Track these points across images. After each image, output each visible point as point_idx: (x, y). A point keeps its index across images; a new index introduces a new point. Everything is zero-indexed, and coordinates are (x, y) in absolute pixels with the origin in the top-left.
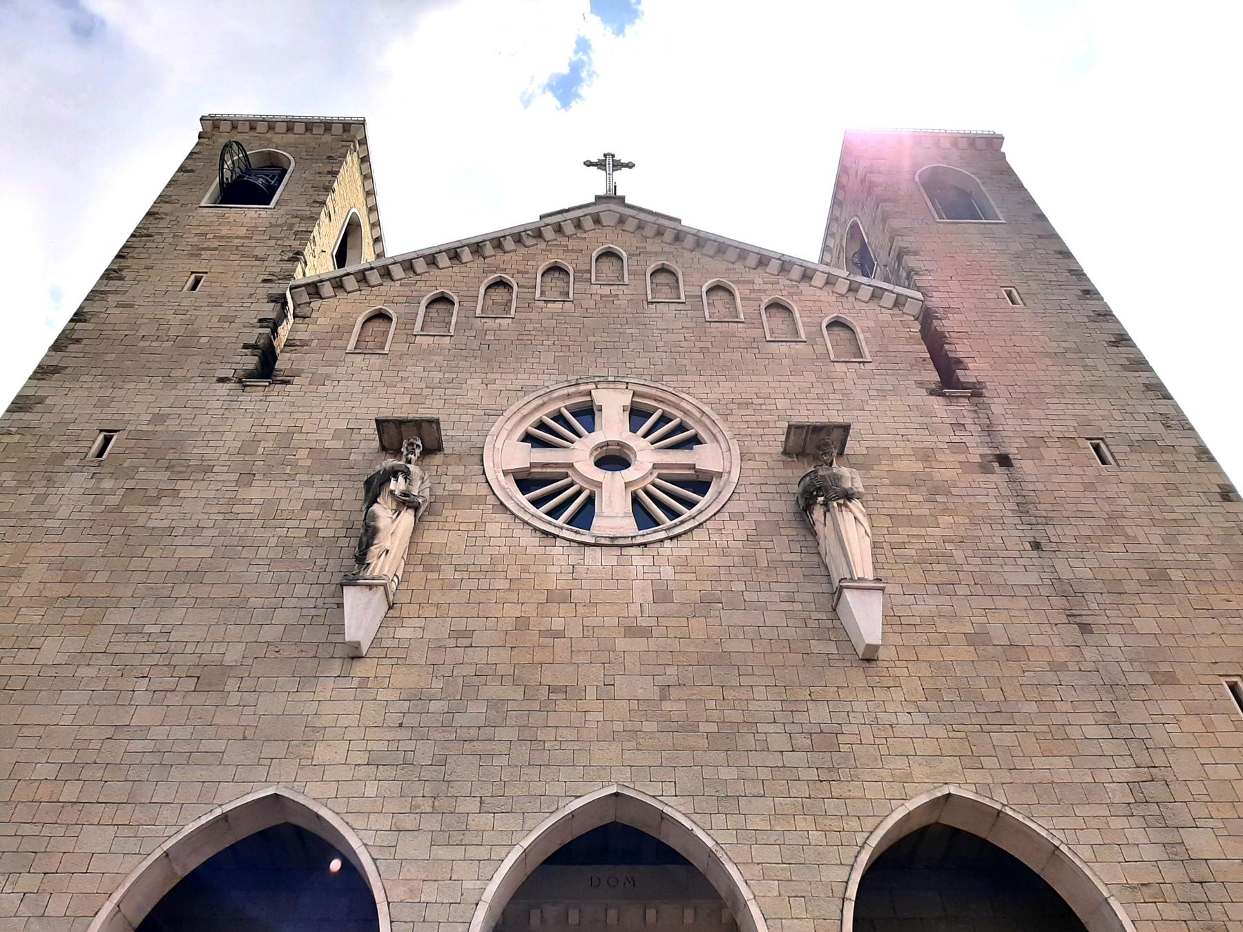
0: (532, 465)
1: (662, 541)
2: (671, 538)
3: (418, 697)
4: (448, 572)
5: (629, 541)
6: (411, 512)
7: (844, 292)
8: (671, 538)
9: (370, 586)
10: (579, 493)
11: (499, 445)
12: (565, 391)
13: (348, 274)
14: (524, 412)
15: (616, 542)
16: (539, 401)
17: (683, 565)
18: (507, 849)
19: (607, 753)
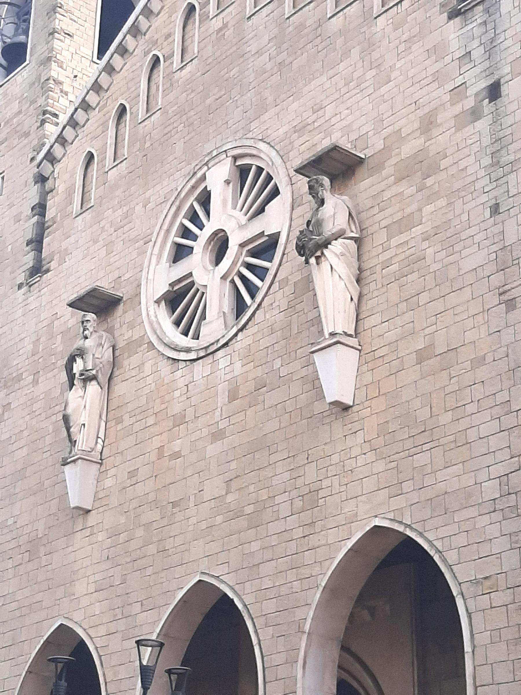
0: (172, 285)
1: (236, 335)
2: (241, 330)
3: (114, 534)
4: (127, 421)
5: (215, 347)
6: (94, 382)
7: (63, 151)
8: (241, 330)
9: (74, 461)
10: (243, 278)
11: (150, 277)
12: (189, 186)
13: (64, 128)
14: (165, 227)
15: (209, 351)
16: (174, 208)
17: (248, 356)
18: (25, 664)
19: (198, 549)
